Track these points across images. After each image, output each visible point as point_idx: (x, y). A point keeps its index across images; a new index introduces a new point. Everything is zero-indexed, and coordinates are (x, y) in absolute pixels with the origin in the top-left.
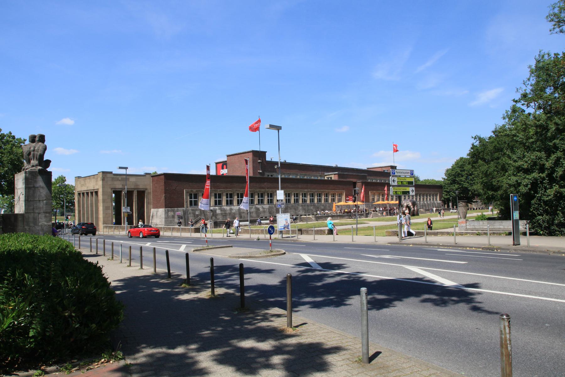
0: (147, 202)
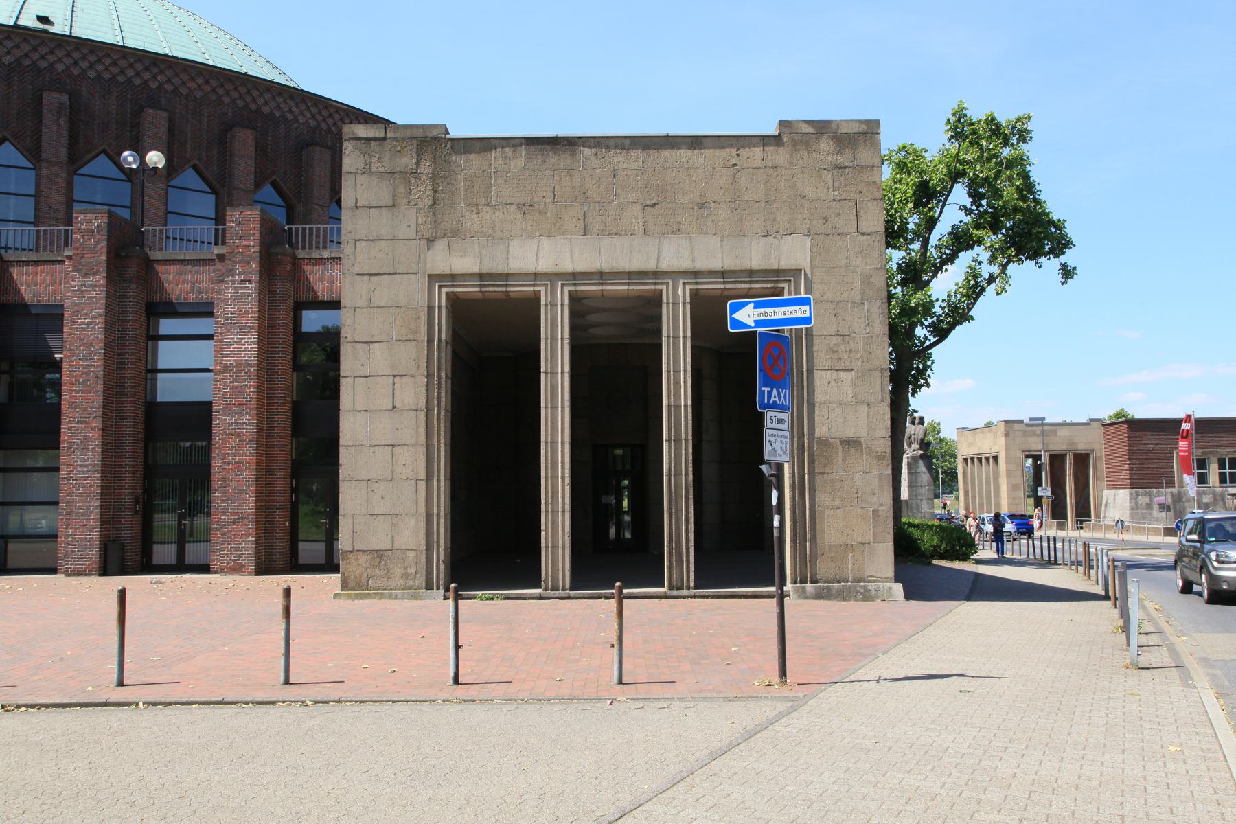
0: (1094, 476)
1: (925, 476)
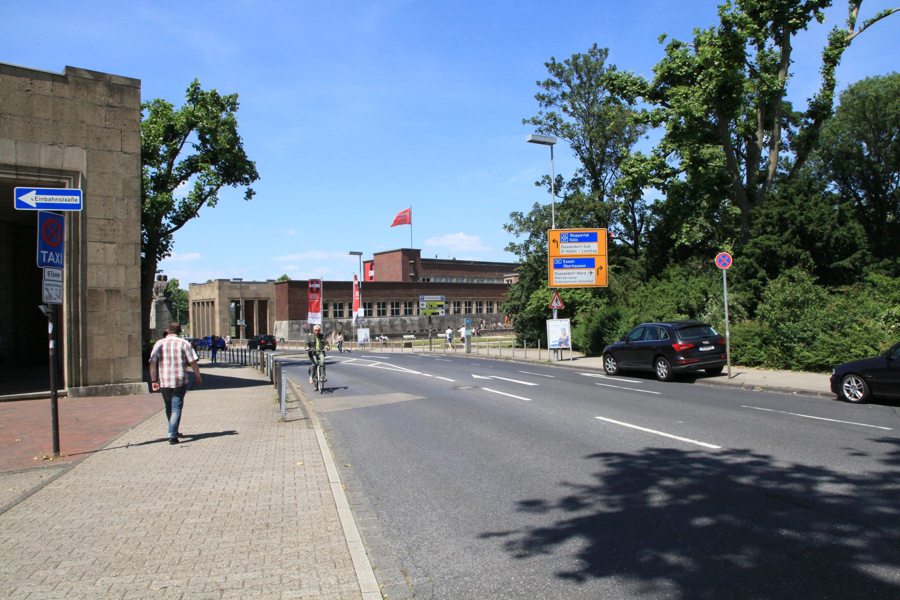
1: (167, 314)
